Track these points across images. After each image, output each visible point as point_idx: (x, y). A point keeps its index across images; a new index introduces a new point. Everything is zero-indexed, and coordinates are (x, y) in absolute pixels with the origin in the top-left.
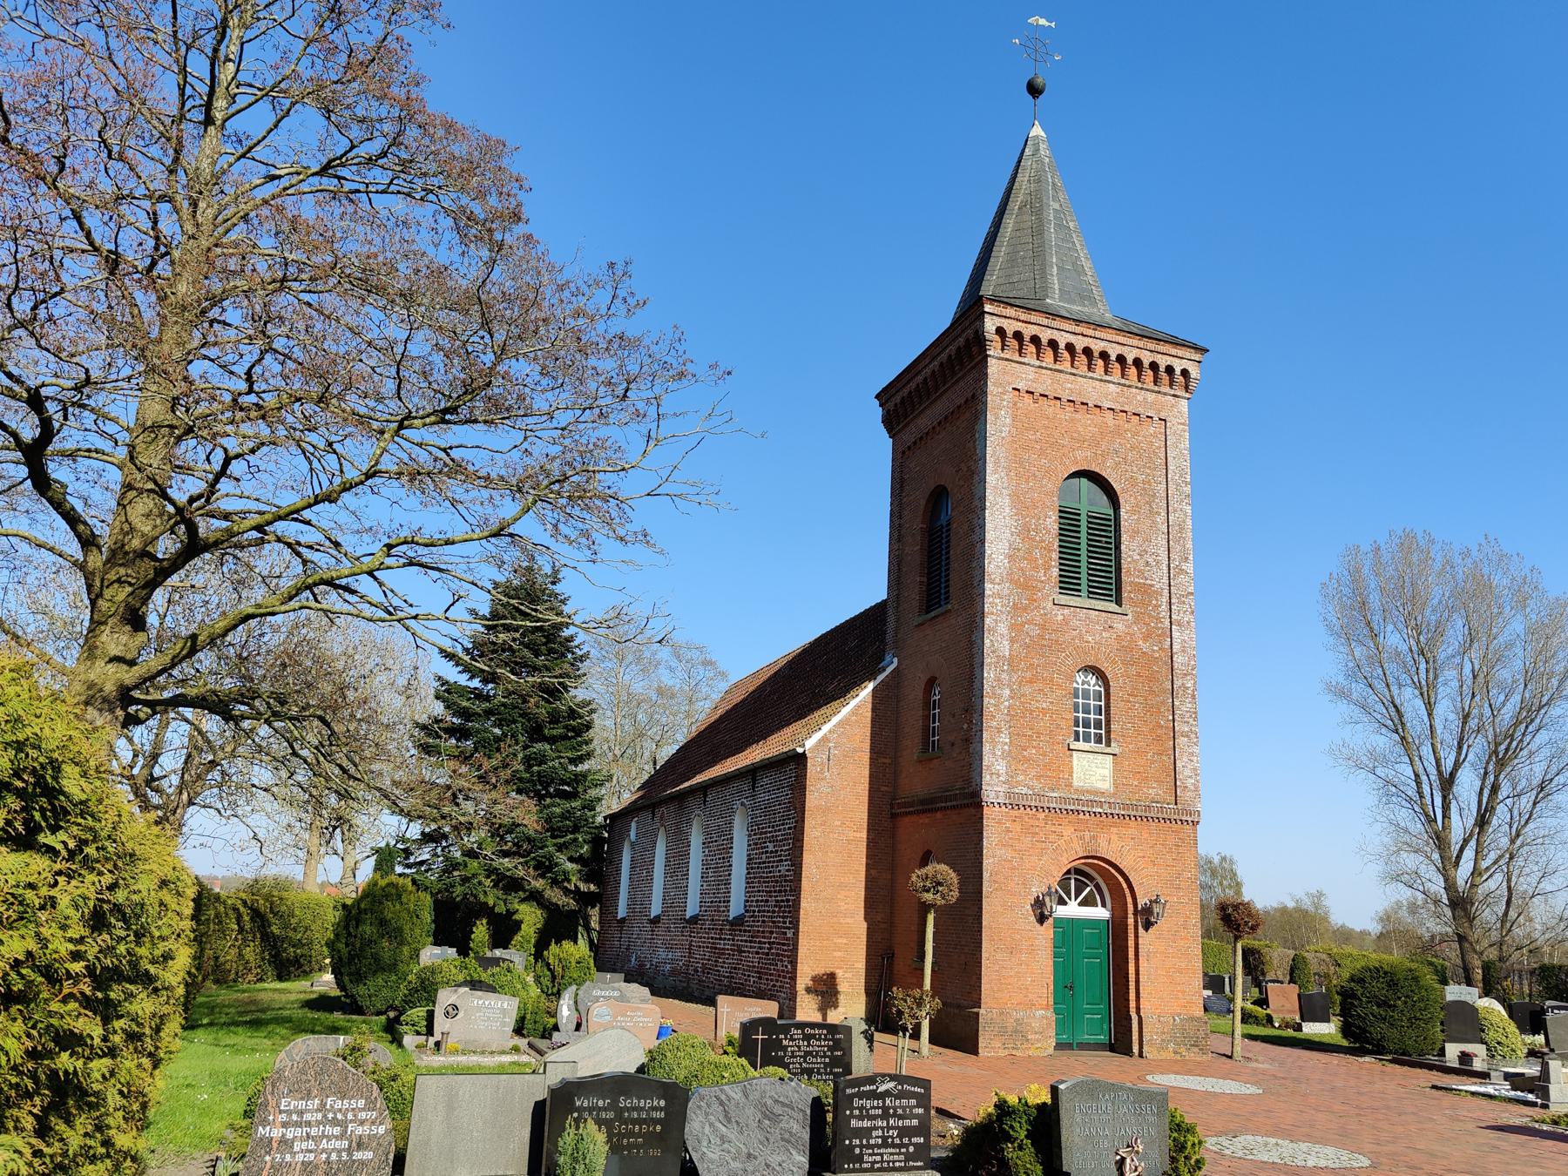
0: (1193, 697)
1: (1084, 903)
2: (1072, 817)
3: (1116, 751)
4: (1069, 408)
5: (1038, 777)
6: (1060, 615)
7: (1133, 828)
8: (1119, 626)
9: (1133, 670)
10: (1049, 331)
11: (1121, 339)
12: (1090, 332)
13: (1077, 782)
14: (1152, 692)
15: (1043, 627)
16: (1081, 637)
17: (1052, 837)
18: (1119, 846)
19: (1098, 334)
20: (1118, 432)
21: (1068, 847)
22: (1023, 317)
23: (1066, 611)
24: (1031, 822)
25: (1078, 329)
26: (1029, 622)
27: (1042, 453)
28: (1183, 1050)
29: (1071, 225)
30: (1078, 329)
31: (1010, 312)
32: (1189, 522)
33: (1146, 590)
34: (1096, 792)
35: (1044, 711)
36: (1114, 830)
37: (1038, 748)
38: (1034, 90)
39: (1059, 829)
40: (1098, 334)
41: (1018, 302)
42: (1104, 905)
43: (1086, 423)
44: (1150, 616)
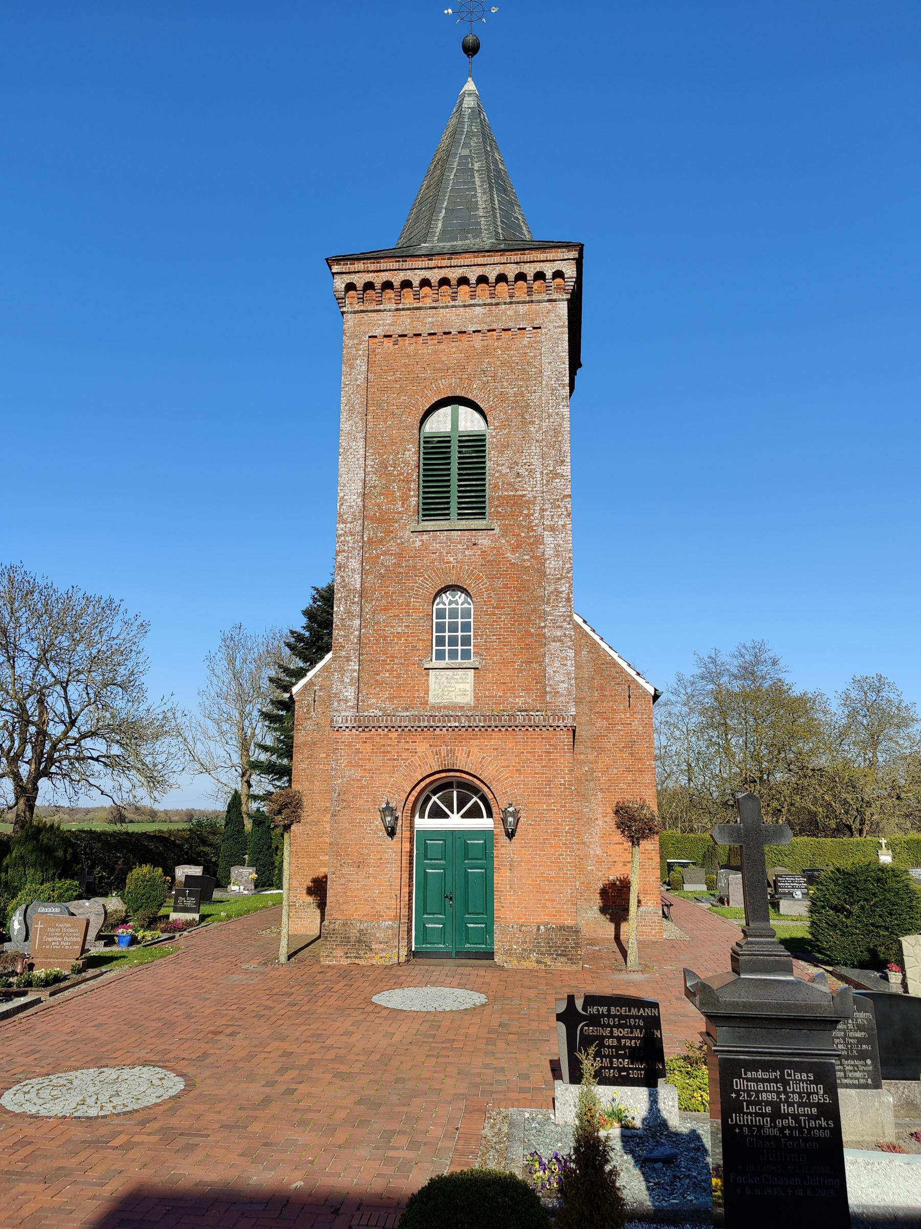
0: (568, 600)
1: (470, 814)
2: (427, 733)
3: (477, 665)
4: (432, 341)
5: (391, 699)
6: (417, 541)
7: (496, 739)
8: (484, 541)
9: (499, 583)
10: (402, 274)
11: (480, 260)
12: (446, 263)
13: (432, 699)
14: (520, 601)
15: (399, 556)
16: (441, 559)
17: (405, 755)
18: (473, 758)
19: (454, 262)
20: (487, 351)
21: (425, 759)
22: (372, 267)
23: (425, 537)
24: (383, 742)
25: (432, 264)
26: (385, 553)
27: (402, 390)
28: (548, 960)
29: (476, 166)
30: (432, 264)
31: (359, 266)
32: (567, 425)
33: (518, 503)
34: (455, 707)
35: (399, 635)
36: (476, 742)
37: (391, 671)
38: (471, 50)
39: (410, 746)
40: (454, 262)
41: (369, 255)
42: (490, 815)
43: (451, 351)
44: (520, 526)
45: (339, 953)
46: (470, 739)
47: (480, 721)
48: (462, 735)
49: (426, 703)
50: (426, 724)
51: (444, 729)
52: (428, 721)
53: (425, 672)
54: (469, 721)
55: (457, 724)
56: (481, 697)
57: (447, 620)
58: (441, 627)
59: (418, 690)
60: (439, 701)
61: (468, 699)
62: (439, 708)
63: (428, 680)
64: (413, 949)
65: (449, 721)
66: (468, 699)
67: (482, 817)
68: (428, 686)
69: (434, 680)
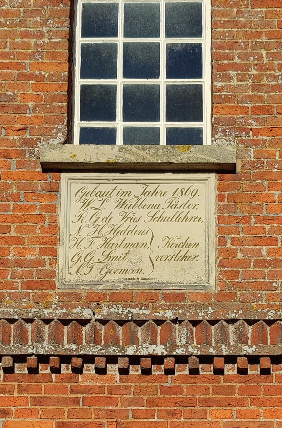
2: (48, 382)
34: (151, 296)
45: (30, 106)
46: (207, 402)
47: (242, 339)
48: (178, 390)
49: (47, 282)
50: (45, 348)
51: (113, 369)
52: (56, 339)
53: (42, 182)
54: (205, 340)
55: (159, 350)
56: (244, 264)
57: (120, 40)
58: (98, 62)
59: (19, 241)
60: (94, 276)
61: (200, 271)
62: (95, 299)
63: (53, 209)
64: (50, 357)
65: (132, 340)
66: (200, 271)
67: (126, 7)
68: (54, 226)
69: (76, 208)
